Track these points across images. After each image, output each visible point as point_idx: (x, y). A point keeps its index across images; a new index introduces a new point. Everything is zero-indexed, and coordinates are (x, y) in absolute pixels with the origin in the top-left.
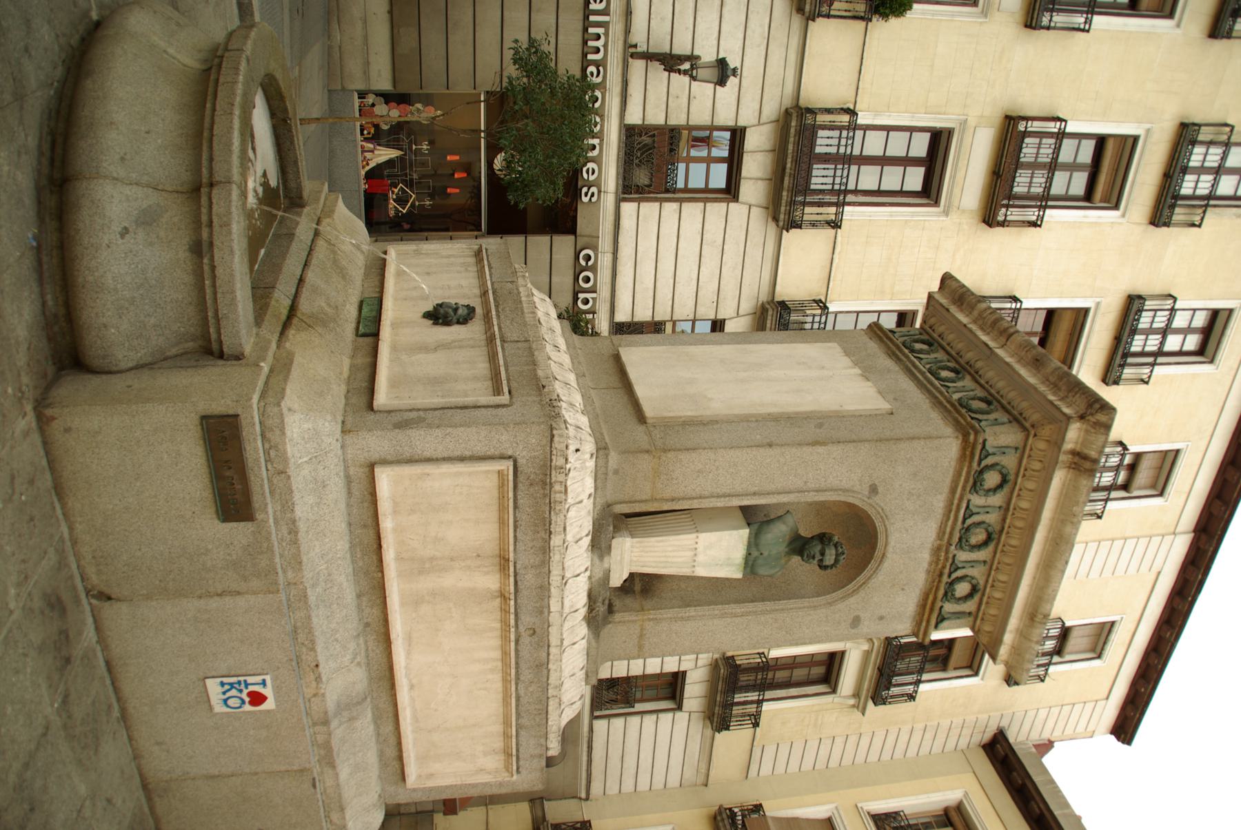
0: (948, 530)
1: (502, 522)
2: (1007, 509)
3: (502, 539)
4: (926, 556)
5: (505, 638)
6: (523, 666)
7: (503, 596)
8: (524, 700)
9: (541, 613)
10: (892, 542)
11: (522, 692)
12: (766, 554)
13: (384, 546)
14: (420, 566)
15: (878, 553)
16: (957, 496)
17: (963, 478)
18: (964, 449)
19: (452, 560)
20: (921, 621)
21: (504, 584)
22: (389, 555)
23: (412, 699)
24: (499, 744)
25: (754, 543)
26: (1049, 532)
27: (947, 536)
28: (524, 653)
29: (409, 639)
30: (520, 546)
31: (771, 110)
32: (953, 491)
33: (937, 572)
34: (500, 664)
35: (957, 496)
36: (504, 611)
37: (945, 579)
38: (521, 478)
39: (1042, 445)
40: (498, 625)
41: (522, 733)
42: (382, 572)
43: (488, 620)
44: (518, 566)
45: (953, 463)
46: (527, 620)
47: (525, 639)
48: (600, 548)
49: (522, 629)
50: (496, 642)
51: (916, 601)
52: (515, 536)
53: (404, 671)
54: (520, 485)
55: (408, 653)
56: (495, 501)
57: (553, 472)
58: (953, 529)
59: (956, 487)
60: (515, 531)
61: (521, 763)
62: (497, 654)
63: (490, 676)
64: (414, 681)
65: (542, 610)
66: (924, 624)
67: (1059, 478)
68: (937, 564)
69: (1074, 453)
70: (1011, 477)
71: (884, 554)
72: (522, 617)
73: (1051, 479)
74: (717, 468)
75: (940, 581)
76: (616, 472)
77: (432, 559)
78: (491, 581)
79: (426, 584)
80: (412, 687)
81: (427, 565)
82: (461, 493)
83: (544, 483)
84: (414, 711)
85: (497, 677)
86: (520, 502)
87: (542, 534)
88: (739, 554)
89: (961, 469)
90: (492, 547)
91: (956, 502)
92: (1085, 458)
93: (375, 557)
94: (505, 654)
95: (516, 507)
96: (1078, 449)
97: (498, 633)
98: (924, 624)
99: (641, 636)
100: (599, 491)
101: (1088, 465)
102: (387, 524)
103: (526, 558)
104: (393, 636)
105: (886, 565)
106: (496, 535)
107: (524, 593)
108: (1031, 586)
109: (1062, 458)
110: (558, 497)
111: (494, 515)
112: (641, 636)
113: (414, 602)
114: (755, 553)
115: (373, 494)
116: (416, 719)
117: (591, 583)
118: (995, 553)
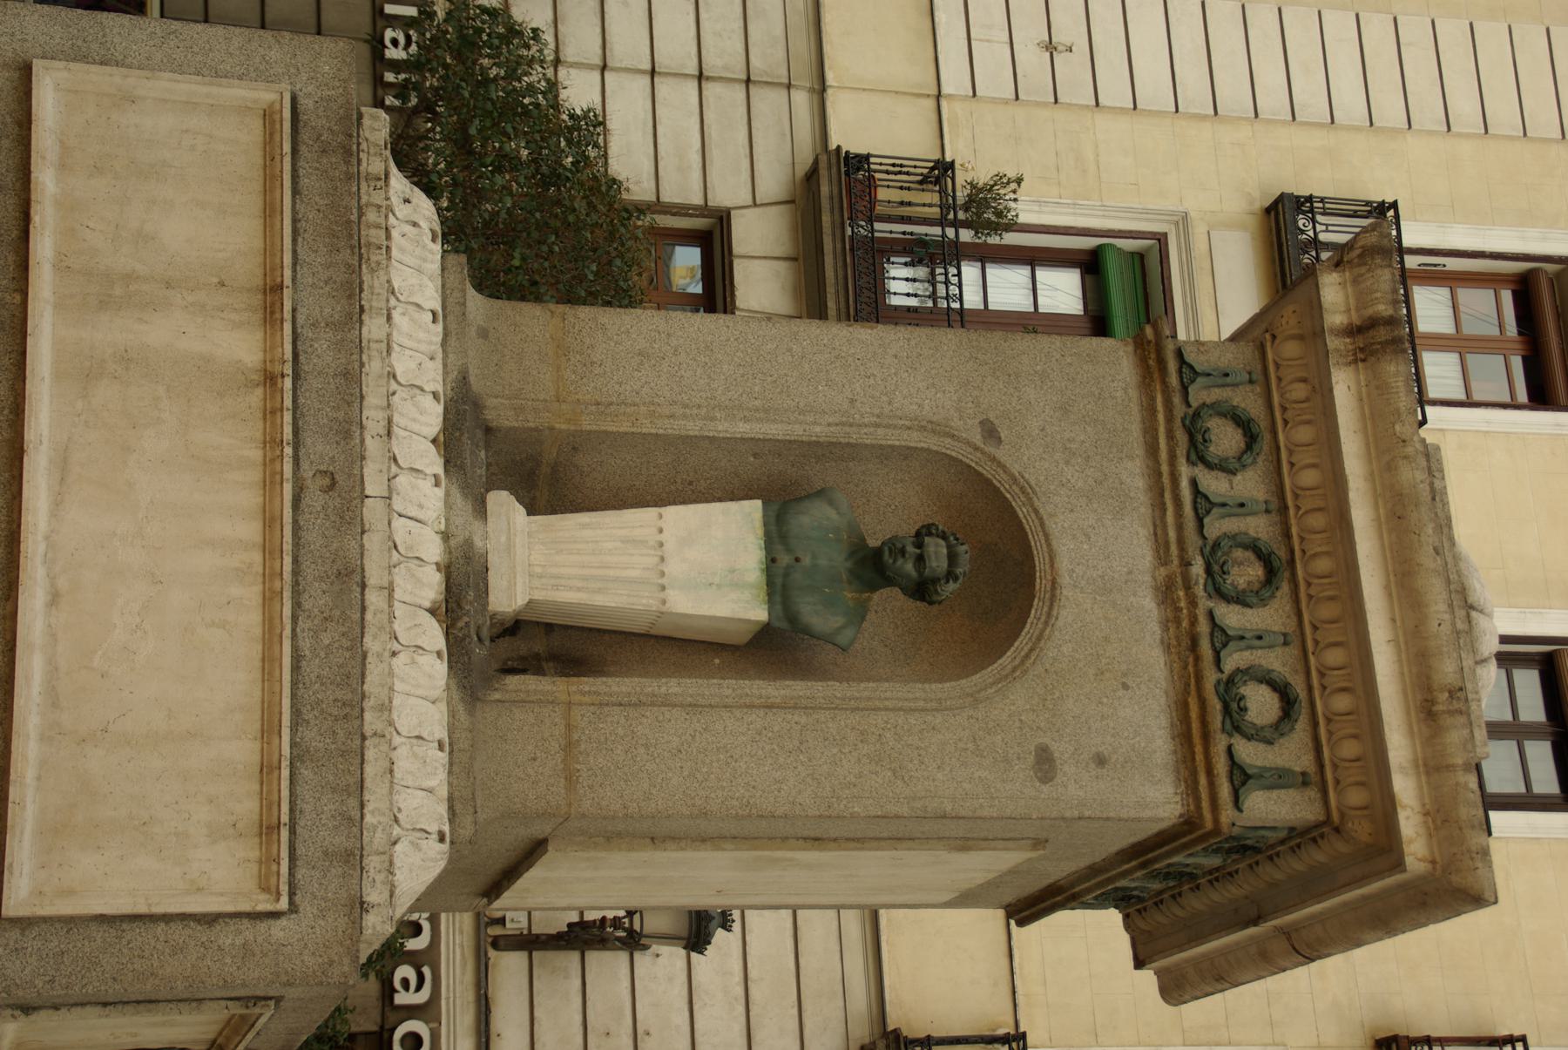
0: (1172, 534)
1: (270, 212)
2: (1284, 509)
3: (270, 250)
4: (1147, 604)
5: (270, 482)
6: (309, 570)
7: (270, 379)
8: (311, 668)
9: (347, 435)
10: (1063, 564)
11: (306, 645)
12: (807, 561)
13: (36, 219)
14: (107, 292)
15: (1041, 584)
16: (1164, 455)
17: (1161, 417)
18: (1143, 361)
19: (168, 285)
20: (1194, 774)
21: (269, 347)
22: (43, 247)
23: (52, 636)
24: (247, 808)
25: (777, 534)
26: (1376, 507)
27: (1174, 549)
28: (312, 537)
29: (62, 465)
30: (305, 277)
31: (774, 180)
32: (1152, 450)
33: (1186, 642)
34: (257, 557)
35: (1164, 455)
36: (271, 413)
37: (1211, 677)
38: (305, 135)
39: (1291, 349)
40: (256, 454)
41: (306, 772)
42: (25, 293)
43: (233, 437)
44: (301, 320)
45: (1134, 393)
46: (319, 448)
47: (315, 499)
48: (462, 468)
49: (307, 471)
50: (251, 499)
51: (1164, 721)
52: (294, 252)
53: (42, 547)
54: (303, 149)
55: (57, 503)
56: (257, 174)
57: (364, 185)
58: (1180, 528)
59: (1156, 438)
60: (294, 241)
61: (301, 873)
62: (251, 530)
63: (236, 591)
64: (62, 583)
65: (348, 430)
66: (1203, 780)
67: (1344, 387)
68: (1178, 621)
69: (1352, 331)
70: (1263, 424)
71: (1054, 582)
72: (307, 439)
73: (1331, 390)
74: (676, 352)
75: (1197, 659)
76: (483, 333)
77: (129, 277)
78: (242, 347)
79: (111, 333)
80: (54, 599)
81: (118, 291)
82: (193, 148)
83: (348, 152)
84: (52, 669)
85: (251, 594)
86: (304, 182)
87: (345, 254)
88: (750, 558)
89: (1153, 399)
90: (248, 270)
91: (1165, 468)
92: (1372, 323)
93: (11, 258)
94: (270, 521)
95: (295, 192)
96: (1356, 321)
97: (255, 475)
98: (1203, 780)
99: (569, 747)
100: (452, 341)
101: (1382, 334)
102: (45, 179)
103: (312, 301)
104: (30, 435)
105: (1066, 615)
106: (258, 243)
107: (312, 383)
108: (1394, 641)
109: (1333, 343)
110: (377, 236)
111: (254, 203)
112: (569, 747)
113: (85, 372)
114: (784, 559)
115: (24, 122)
116: (53, 699)
117: (448, 551)
118: (1315, 724)
